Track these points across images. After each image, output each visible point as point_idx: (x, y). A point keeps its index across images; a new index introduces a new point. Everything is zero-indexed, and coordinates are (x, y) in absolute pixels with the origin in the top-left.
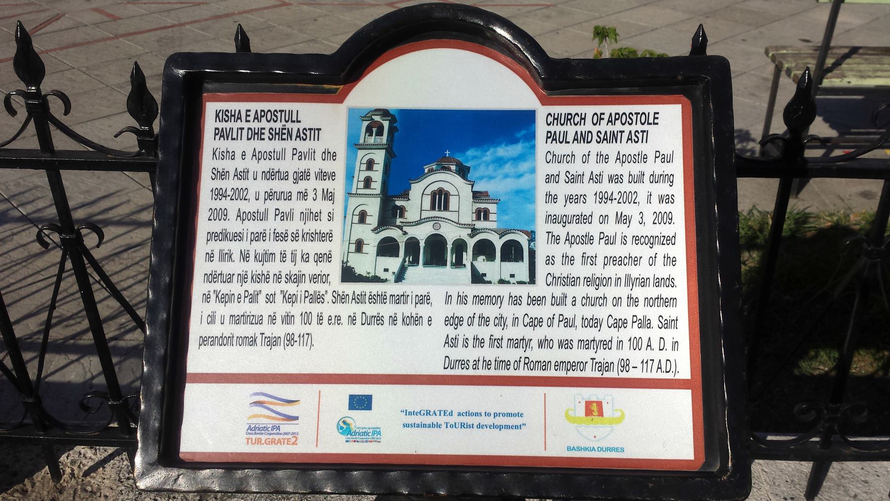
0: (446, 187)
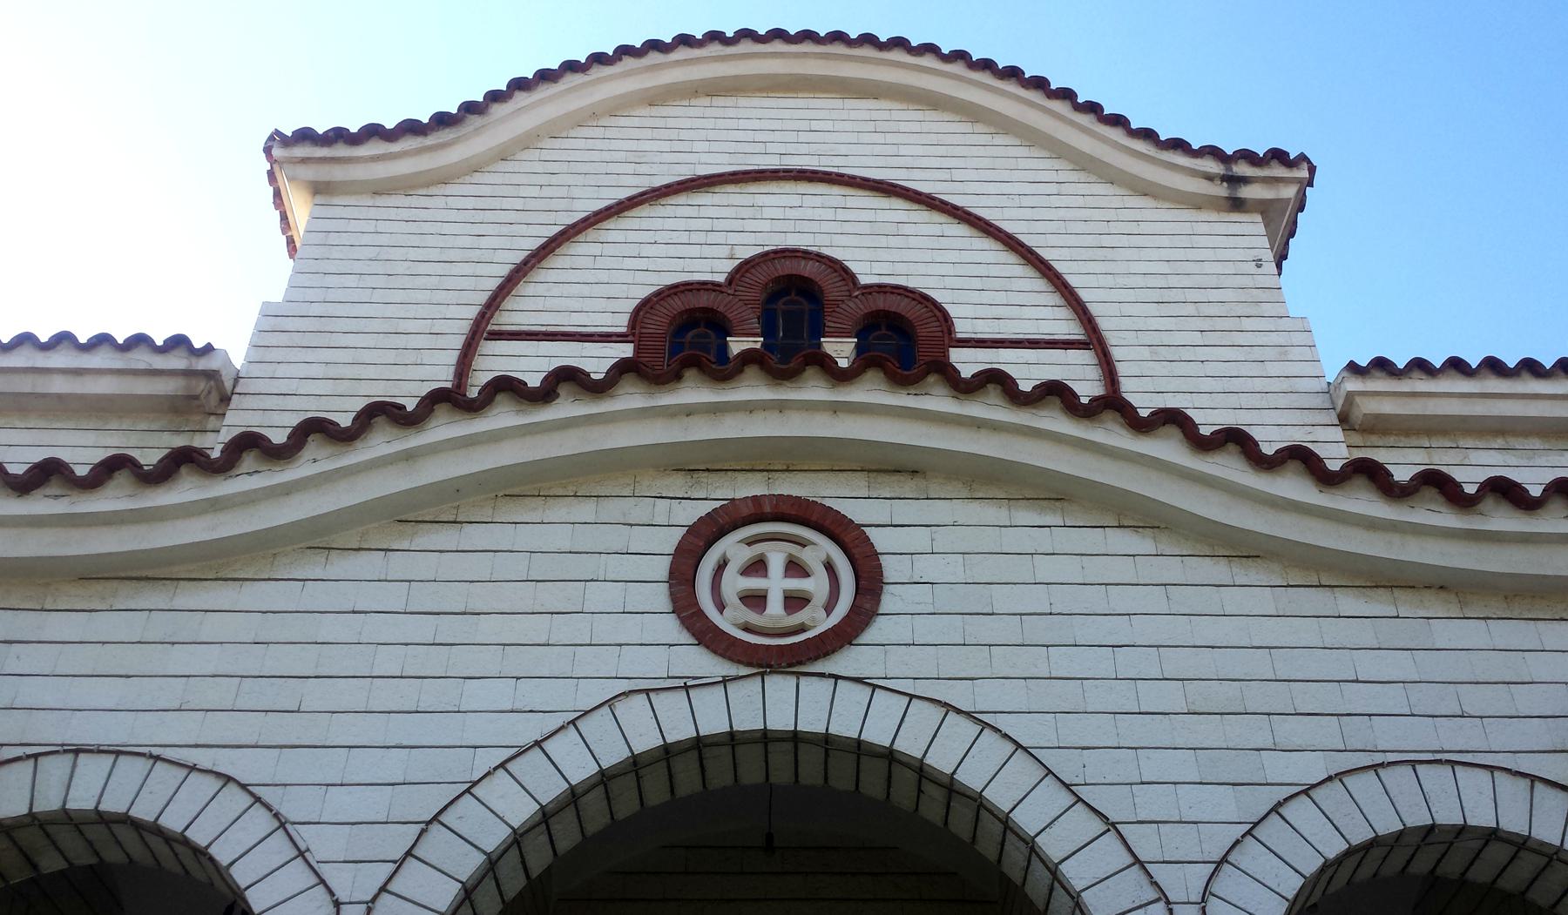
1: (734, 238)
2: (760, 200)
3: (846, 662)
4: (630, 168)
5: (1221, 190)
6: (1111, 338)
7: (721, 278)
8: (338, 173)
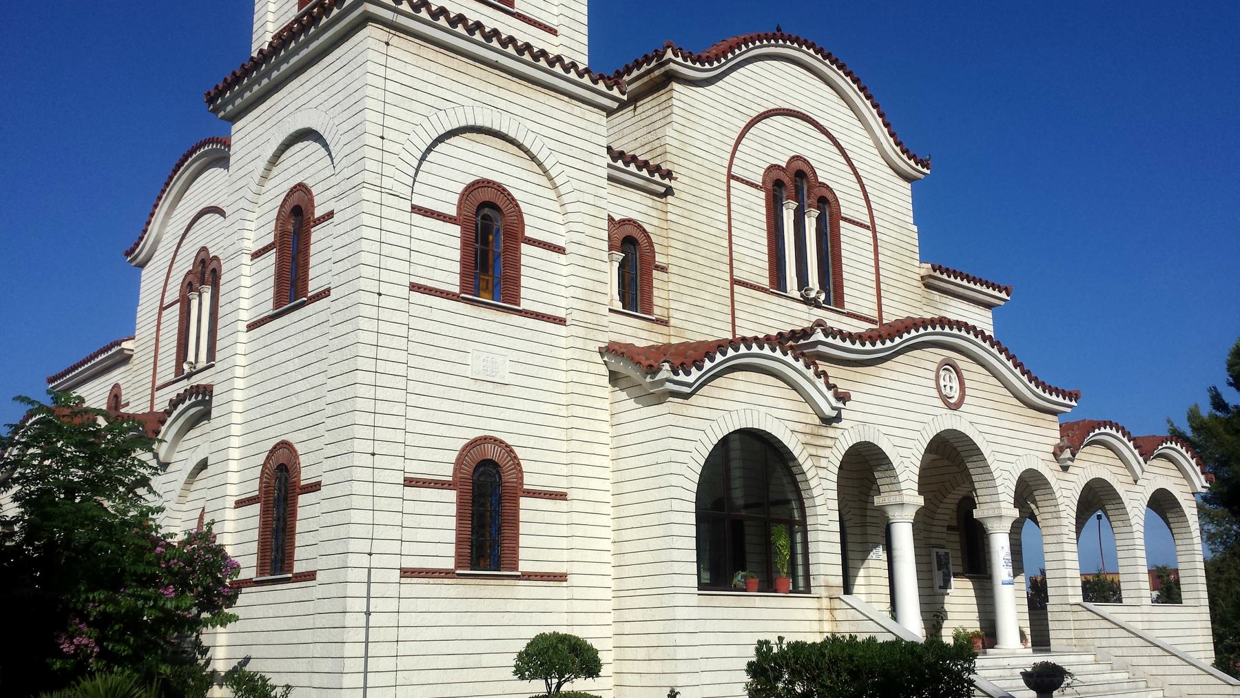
0: (830, 171)
3: (963, 408)
6: (878, 229)
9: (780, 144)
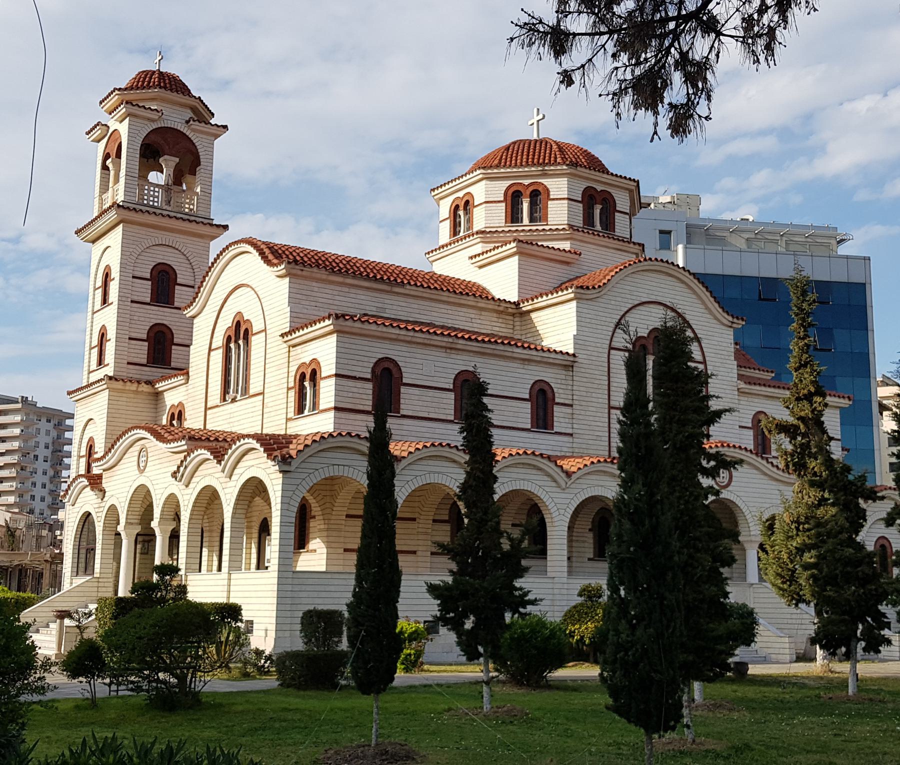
1: (648, 323)
2: (653, 310)
4: (629, 296)
5: (730, 324)
7: (646, 335)
8: (584, 297)
9: (645, 322)
